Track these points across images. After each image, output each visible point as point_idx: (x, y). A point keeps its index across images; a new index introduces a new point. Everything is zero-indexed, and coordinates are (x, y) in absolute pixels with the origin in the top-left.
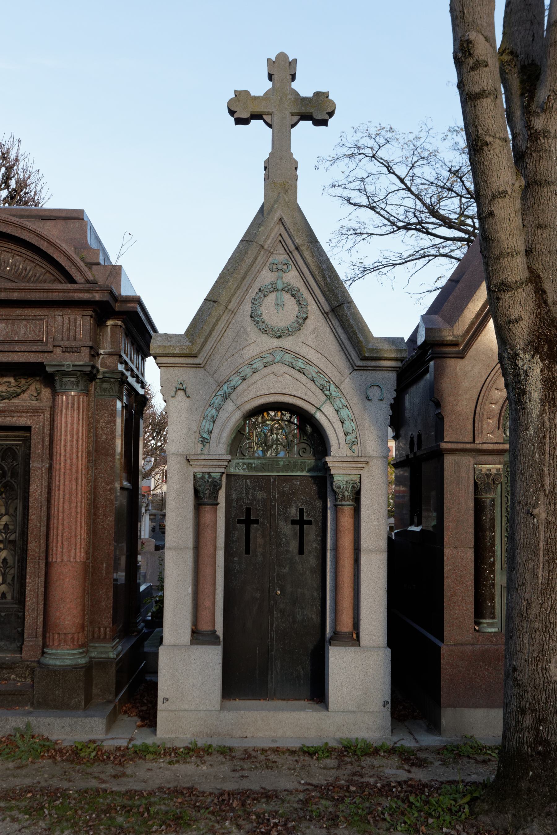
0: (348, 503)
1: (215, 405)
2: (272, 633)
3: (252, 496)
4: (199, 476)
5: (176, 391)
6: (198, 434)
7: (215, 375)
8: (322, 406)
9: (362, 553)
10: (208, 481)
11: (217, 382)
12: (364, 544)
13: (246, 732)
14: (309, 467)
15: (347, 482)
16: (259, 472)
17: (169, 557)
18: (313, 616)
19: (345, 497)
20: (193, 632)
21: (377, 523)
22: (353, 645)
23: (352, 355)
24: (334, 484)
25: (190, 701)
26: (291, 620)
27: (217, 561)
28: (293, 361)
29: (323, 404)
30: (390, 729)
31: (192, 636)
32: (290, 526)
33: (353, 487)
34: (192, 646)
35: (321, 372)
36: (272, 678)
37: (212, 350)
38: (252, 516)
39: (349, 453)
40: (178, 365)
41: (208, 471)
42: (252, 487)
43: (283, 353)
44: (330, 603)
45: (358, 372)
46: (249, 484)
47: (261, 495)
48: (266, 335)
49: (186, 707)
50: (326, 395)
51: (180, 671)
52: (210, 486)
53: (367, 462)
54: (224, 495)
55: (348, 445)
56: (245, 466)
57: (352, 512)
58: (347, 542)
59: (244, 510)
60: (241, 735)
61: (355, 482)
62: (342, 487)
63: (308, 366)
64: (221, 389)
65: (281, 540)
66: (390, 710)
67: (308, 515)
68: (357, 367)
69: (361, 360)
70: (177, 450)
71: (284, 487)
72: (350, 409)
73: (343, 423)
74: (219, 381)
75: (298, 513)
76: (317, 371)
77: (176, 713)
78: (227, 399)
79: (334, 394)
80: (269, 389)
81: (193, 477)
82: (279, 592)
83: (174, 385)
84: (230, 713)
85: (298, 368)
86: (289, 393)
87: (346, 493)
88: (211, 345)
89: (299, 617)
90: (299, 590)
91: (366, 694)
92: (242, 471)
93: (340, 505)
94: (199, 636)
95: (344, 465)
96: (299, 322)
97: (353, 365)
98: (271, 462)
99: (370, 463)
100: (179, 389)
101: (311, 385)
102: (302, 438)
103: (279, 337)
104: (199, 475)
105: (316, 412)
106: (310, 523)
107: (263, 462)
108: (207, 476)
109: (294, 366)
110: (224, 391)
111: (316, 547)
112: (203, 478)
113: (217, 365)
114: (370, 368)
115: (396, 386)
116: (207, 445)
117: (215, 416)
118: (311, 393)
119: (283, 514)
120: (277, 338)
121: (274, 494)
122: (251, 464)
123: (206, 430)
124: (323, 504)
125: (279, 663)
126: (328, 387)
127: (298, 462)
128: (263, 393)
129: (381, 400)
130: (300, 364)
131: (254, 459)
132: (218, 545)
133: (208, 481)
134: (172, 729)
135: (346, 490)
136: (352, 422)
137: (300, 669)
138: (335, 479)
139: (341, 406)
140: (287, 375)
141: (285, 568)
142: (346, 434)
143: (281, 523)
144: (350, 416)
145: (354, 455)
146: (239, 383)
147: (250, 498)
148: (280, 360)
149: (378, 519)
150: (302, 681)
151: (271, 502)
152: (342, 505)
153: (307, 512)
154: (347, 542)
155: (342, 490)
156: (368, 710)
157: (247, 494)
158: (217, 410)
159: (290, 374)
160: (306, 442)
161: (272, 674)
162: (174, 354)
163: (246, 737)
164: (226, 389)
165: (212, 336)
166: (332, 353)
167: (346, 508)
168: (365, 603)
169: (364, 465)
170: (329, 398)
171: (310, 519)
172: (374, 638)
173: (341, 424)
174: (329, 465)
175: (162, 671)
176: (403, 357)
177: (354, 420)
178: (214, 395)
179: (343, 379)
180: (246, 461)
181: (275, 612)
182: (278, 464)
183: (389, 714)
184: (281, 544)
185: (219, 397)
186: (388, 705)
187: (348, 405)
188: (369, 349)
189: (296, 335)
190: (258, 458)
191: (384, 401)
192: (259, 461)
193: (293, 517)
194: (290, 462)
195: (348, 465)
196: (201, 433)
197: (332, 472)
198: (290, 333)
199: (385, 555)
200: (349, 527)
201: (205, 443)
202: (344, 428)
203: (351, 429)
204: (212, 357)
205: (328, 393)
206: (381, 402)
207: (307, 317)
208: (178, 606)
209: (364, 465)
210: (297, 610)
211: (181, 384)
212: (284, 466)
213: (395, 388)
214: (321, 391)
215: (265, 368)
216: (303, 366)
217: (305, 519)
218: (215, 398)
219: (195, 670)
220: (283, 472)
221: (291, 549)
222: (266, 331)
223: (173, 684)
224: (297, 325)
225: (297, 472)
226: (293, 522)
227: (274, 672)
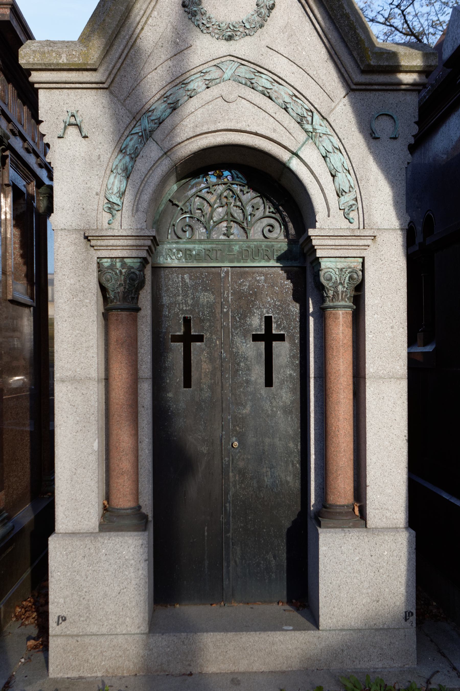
0: (343, 303)
1: (128, 150)
2: (228, 505)
3: (193, 299)
4: (106, 265)
5: (65, 128)
6: (102, 198)
7: (127, 102)
8: (300, 149)
9: (367, 381)
10: (121, 272)
11: (130, 112)
12: (371, 368)
13: (190, 665)
14: (279, 253)
15: (341, 270)
16: (203, 262)
17: (61, 395)
18: (289, 479)
19: (338, 295)
20: (105, 509)
21: (390, 334)
22: (355, 526)
23: (348, 65)
24: (322, 273)
25: (100, 620)
26: (255, 485)
27: (139, 399)
28: (253, 76)
29: (302, 146)
30: (415, 655)
31: (103, 516)
32: (251, 343)
33: (351, 278)
34: (102, 534)
35: (297, 95)
36: (228, 572)
37: (121, 61)
38: (192, 330)
39: (345, 224)
40: (67, 86)
41: (120, 255)
42: (192, 286)
43: (237, 65)
44: (315, 460)
45: (357, 93)
46: (187, 281)
47: (206, 298)
48: (208, 35)
49: (94, 629)
50: (306, 131)
51: (83, 574)
52: (125, 281)
53: (375, 236)
54: (149, 297)
55: (342, 212)
56: (181, 254)
57: (350, 318)
58: (341, 365)
59: (181, 321)
60: (183, 671)
61: (354, 271)
62: (334, 278)
63: (275, 84)
64: (138, 124)
65: (238, 364)
66: (414, 625)
67: (278, 326)
68: (356, 84)
69: (363, 72)
70: (69, 223)
71: (240, 284)
72: (344, 153)
73: (333, 176)
74: (134, 110)
75: (263, 323)
76: (291, 93)
77: (79, 639)
78: (147, 139)
79: (320, 130)
80: (215, 122)
81: (95, 265)
82: (236, 444)
83: (61, 118)
84: (164, 636)
85: (261, 89)
86: (248, 129)
87: (340, 288)
88: (120, 51)
89: (267, 481)
90: (267, 440)
91: (378, 601)
92: (176, 261)
93: (331, 308)
94: (112, 518)
95: (338, 242)
96: (261, 13)
97: (350, 82)
98: (220, 247)
99: (378, 239)
100: (70, 125)
101: (281, 115)
102: (268, 210)
103: (230, 38)
104: (106, 263)
105: (291, 158)
106: (281, 338)
107: (209, 246)
108: (118, 265)
109: (255, 85)
110: (143, 127)
111: (291, 375)
112: (112, 267)
113: (130, 85)
114: (376, 87)
115: (417, 116)
116: (118, 214)
117: (130, 168)
118: (282, 128)
119: (240, 326)
120: (227, 40)
121: (226, 295)
122: (190, 250)
123: (115, 190)
124: (300, 310)
125: (238, 549)
126: (309, 119)
127: (261, 246)
128: (205, 129)
129: (395, 138)
130: (263, 81)
131: (194, 242)
132: (141, 374)
133: (121, 272)
134: (74, 664)
135: (341, 283)
136: (348, 174)
137: (270, 557)
138: (323, 266)
139: (330, 149)
140: (243, 101)
141: (245, 407)
142: (340, 194)
143: (238, 340)
144: (345, 165)
145: (352, 226)
146: (167, 114)
147: (190, 302)
148: (232, 76)
149: (392, 327)
150: (274, 576)
151: (222, 308)
152: (334, 307)
153: (276, 322)
154: (341, 365)
155: (334, 283)
156: (381, 626)
157: (186, 296)
158: (132, 158)
159: (248, 98)
160: (273, 215)
161: (228, 566)
162: (58, 64)
163: (191, 674)
164: (146, 124)
165: (121, 36)
166: (315, 64)
167: (340, 312)
168: (374, 460)
169: (369, 242)
170: (312, 135)
171: (282, 332)
172: (388, 514)
173: (331, 178)
174: (314, 242)
175: (54, 575)
176: (431, 66)
177: (351, 171)
178: (126, 133)
179: (333, 105)
180: (182, 246)
181: (231, 474)
182: (230, 250)
183: (413, 631)
184: (237, 370)
185: (135, 137)
186: (411, 618)
187: (342, 148)
188: (376, 53)
189: (256, 34)
190: (200, 242)
191: (400, 140)
192: (203, 246)
193: (256, 330)
194: (249, 247)
195: (343, 242)
196: (108, 196)
197: (319, 254)
198: (247, 31)
199: (404, 385)
200: (345, 341)
201: (114, 212)
202: (337, 184)
203: (348, 185)
204: (122, 73)
205: (309, 128)
206: (395, 142)
207: (274, 5)
208: (78, 472)
209: (369, 242)
210: (264, 470)
211: (73, 116)
212: (241, 253)
213: (417, 119)
214: (298, 125)
215: (207, 90)
216: (268, 85)
217: (274, 332)
218: (129, 138)
219: (107, 571)
220: (239, 262)
221: (253, 379)
222: (208, 28)
223: (72, 594)
224: (257, 19)
225: (260, 262)
226: (256, 338)
227: (232, 563)
